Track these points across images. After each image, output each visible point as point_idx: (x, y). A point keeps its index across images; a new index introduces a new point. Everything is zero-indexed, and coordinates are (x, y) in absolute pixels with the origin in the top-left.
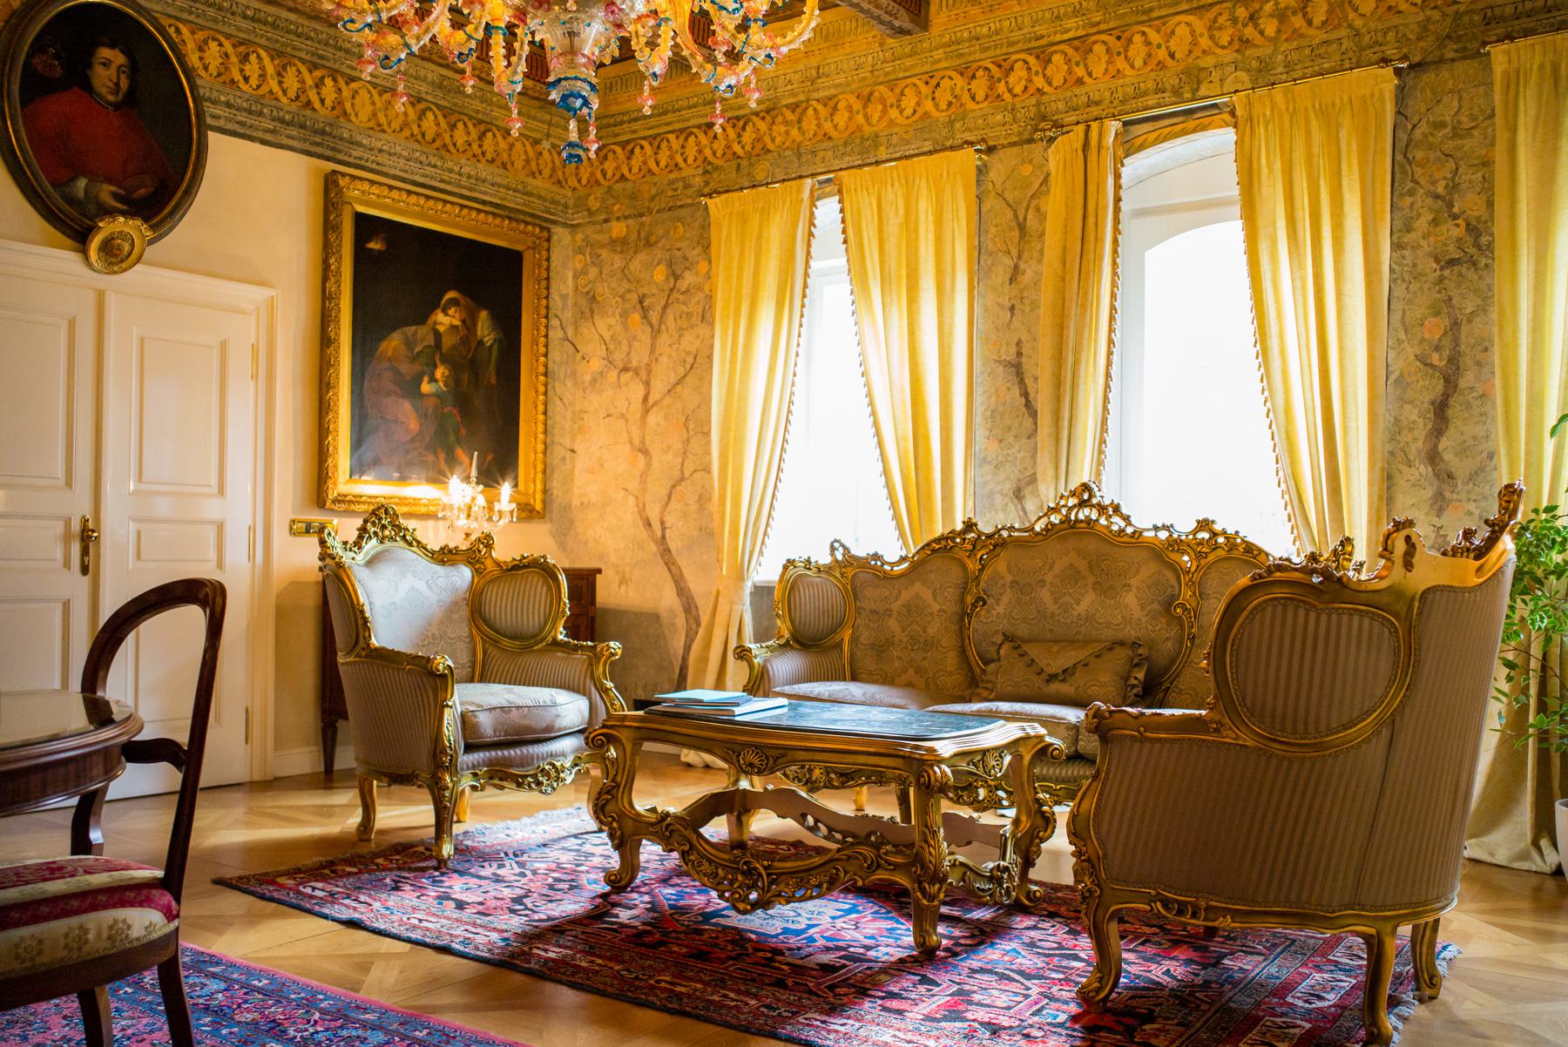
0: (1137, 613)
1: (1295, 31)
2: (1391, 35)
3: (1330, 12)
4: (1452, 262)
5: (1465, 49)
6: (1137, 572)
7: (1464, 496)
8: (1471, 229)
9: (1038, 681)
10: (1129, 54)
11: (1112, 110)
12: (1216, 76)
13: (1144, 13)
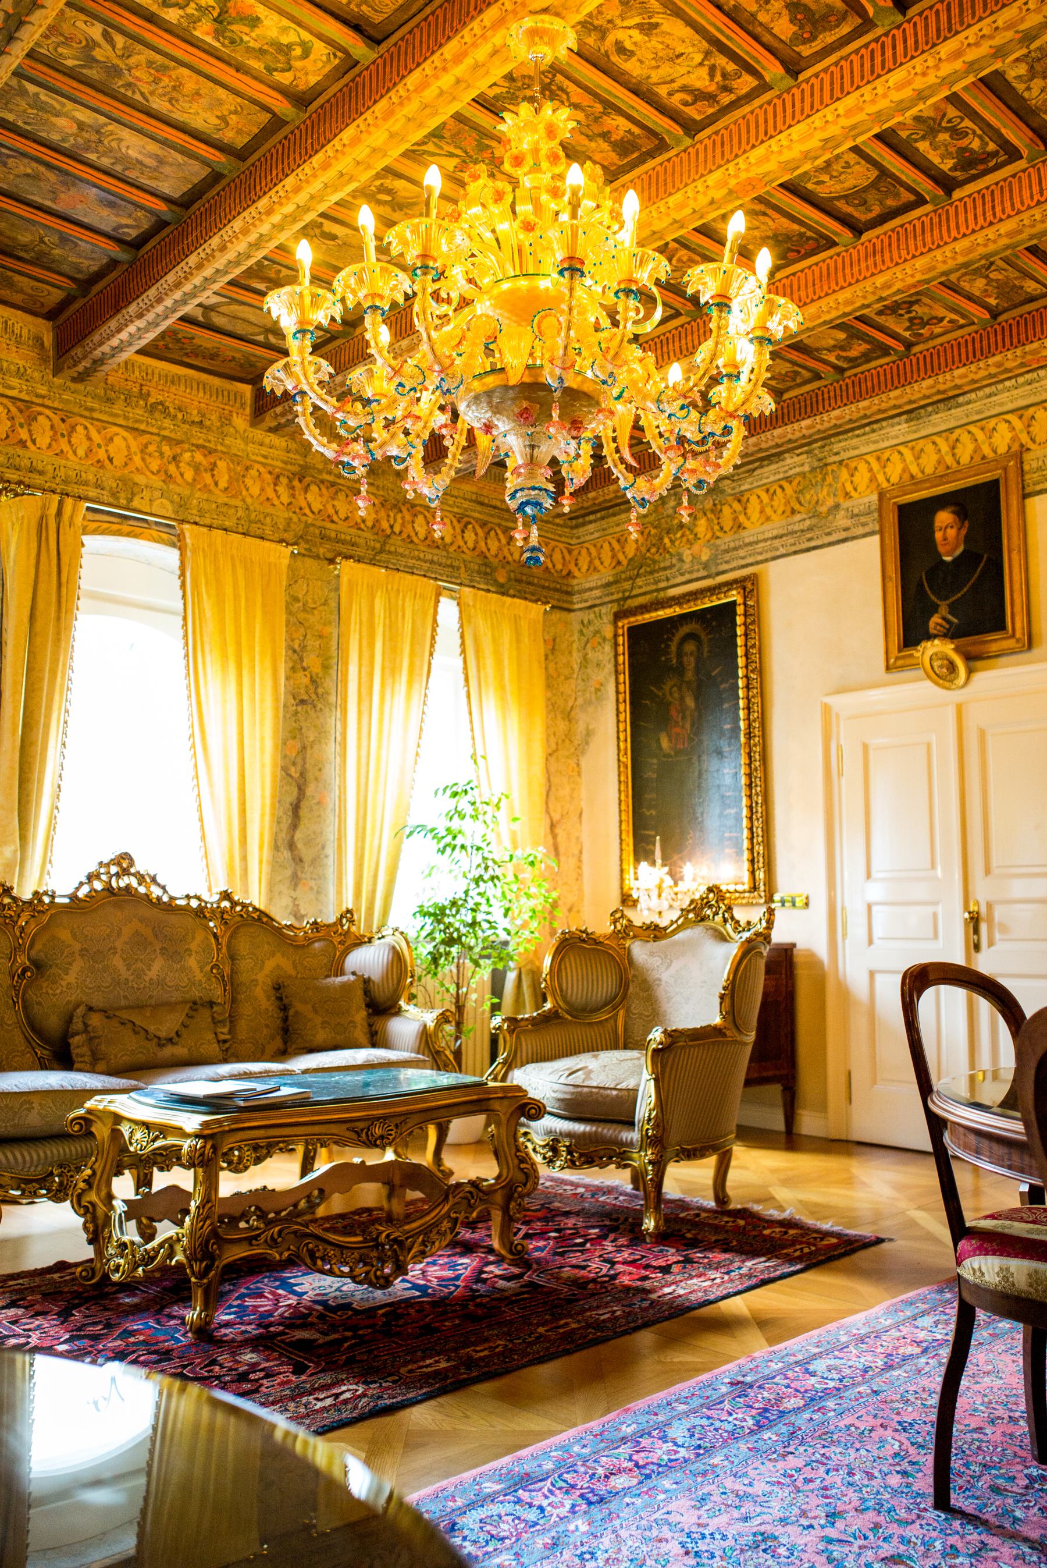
0: (199, 976)
1: (205, 486)
2: (268, 519)
3: (230, 482)
4: (302, 702)
5: (310, 550)
6: (193, 938)
7: (308, 875)
8: (313, 681)
9: (152, 1046)
10: (73, 440)
11: (54, 486)
12: (146, 494)
13: (86, 409)
